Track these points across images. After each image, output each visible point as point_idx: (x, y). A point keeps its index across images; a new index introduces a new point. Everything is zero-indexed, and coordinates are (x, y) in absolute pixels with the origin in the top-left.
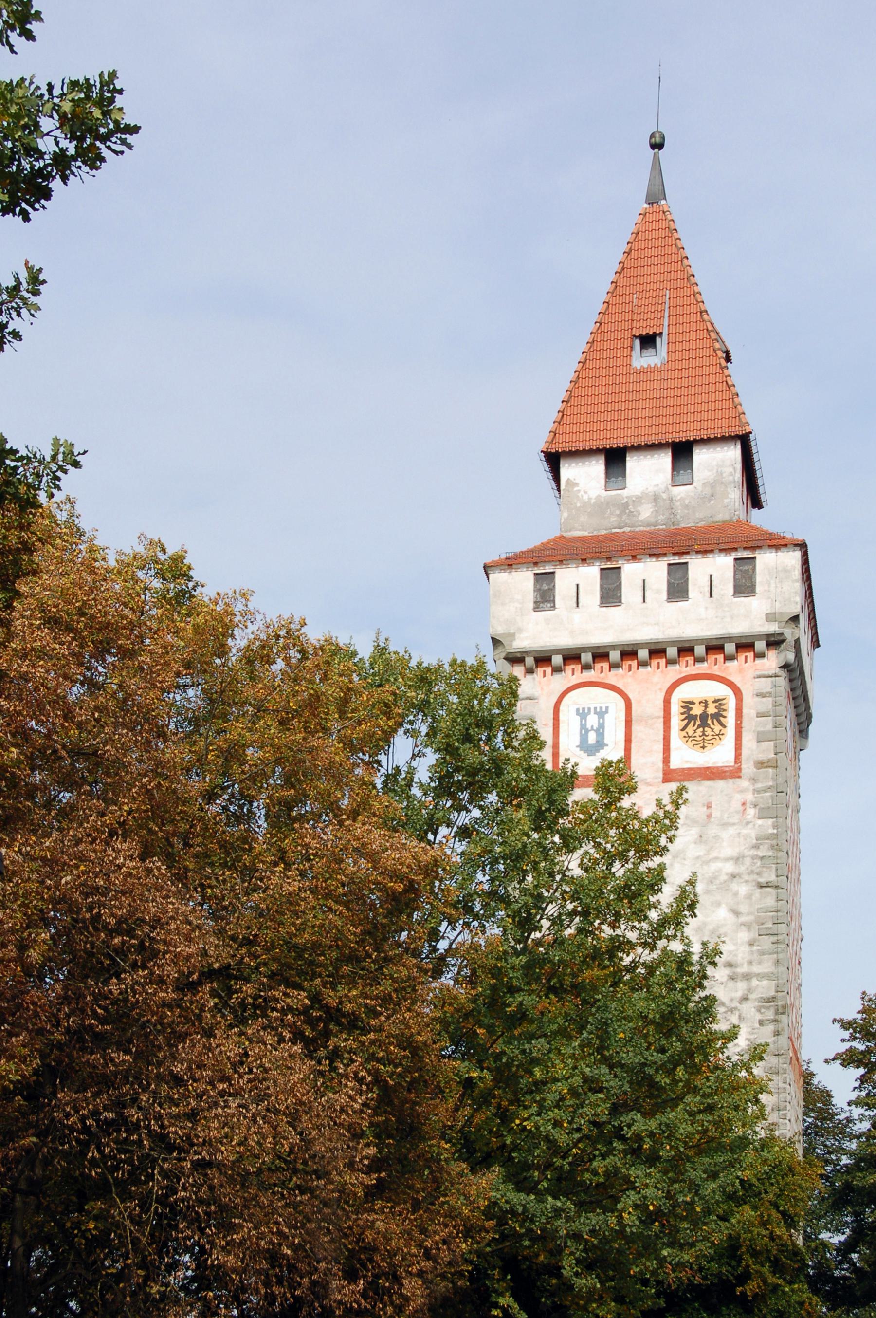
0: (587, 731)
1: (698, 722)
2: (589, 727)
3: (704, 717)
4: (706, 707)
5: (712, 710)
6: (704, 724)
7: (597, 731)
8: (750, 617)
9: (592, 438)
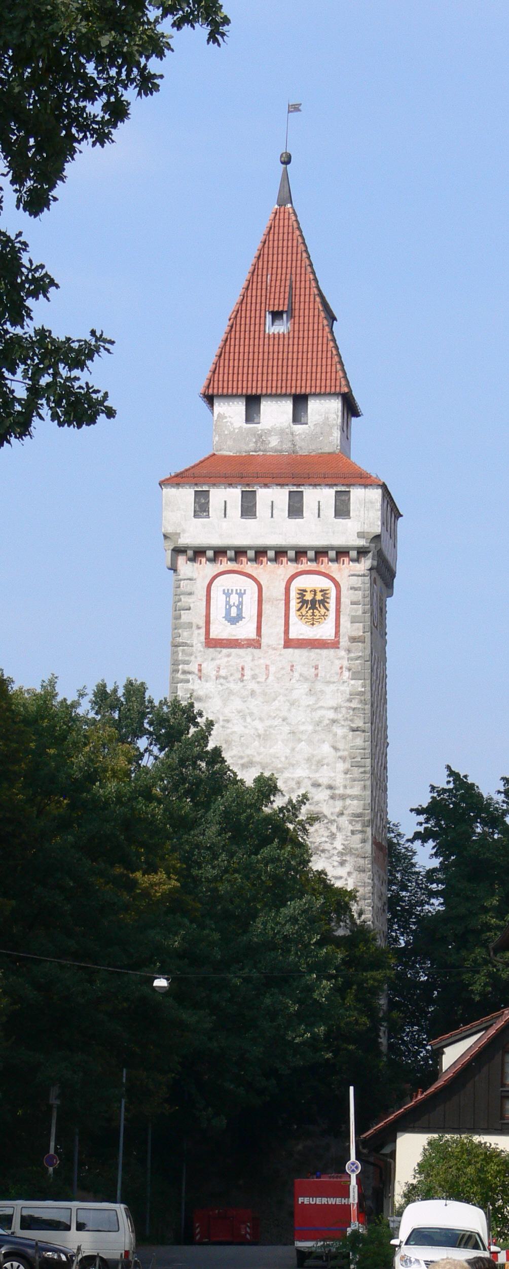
0: (230, 607)
1: (309, 606)
2: (232, 603)
3: (313, 602)
4: (315, 595)
5: (319, 597)
6: (313, 607)
7: (237, 607)
8: (346, 534)
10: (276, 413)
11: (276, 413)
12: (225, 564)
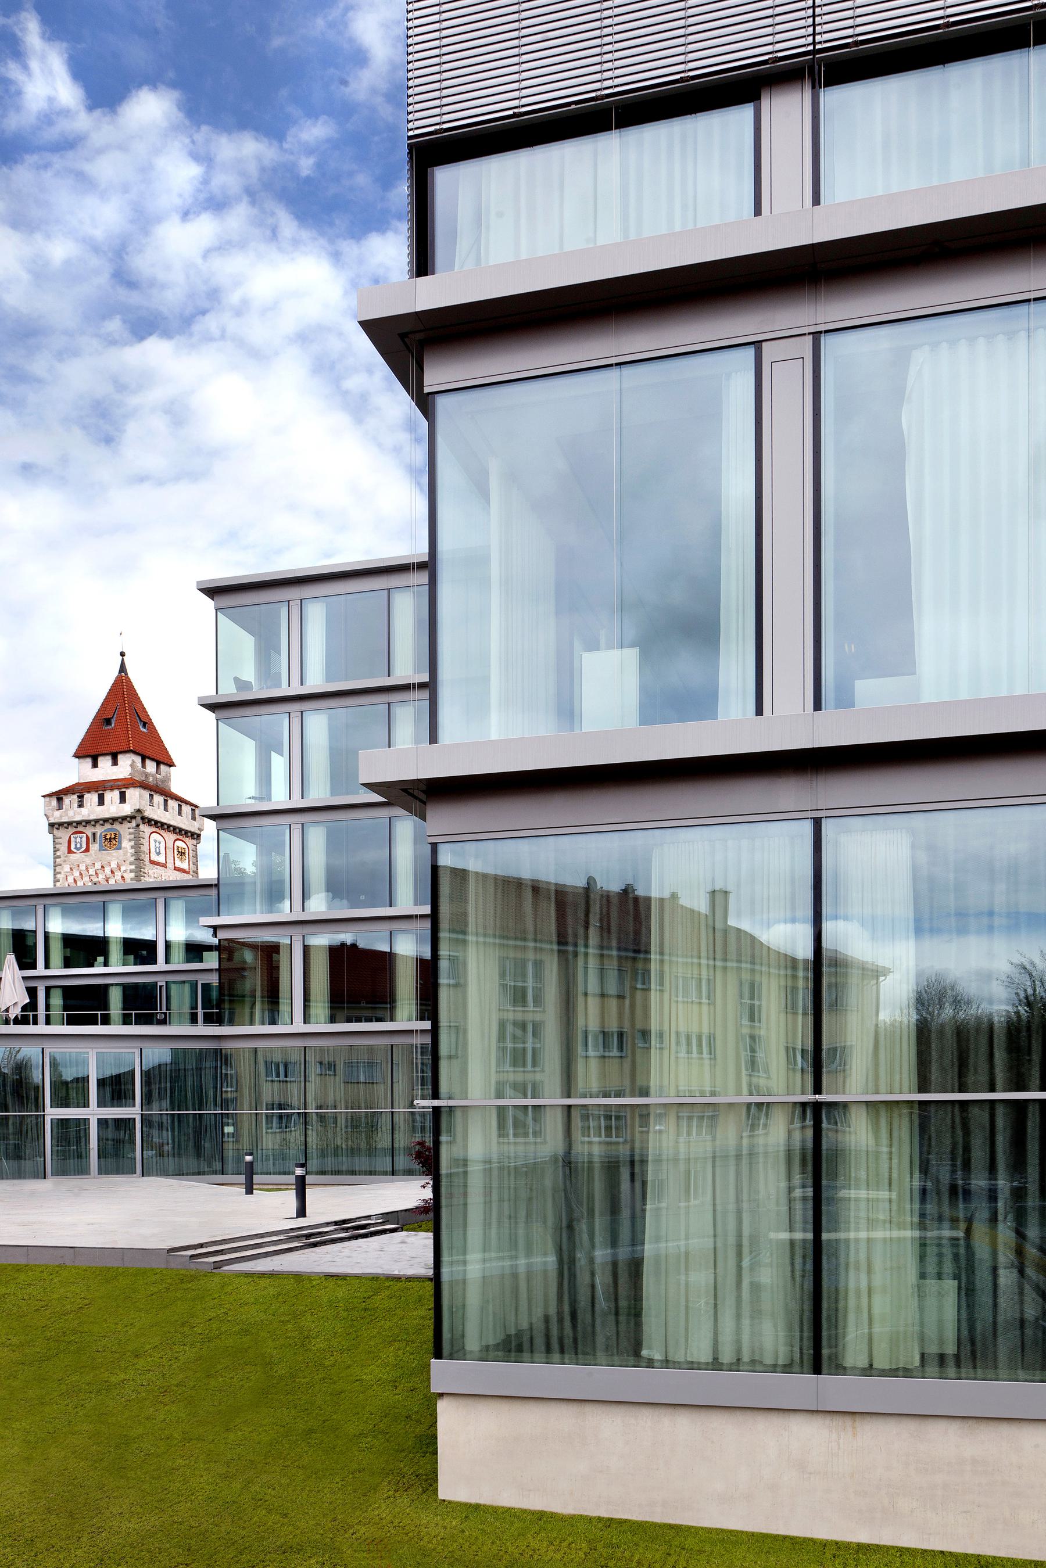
9: (90, 750)
10: (105, 762)
11: (105, 762)
12: (71, 830)
